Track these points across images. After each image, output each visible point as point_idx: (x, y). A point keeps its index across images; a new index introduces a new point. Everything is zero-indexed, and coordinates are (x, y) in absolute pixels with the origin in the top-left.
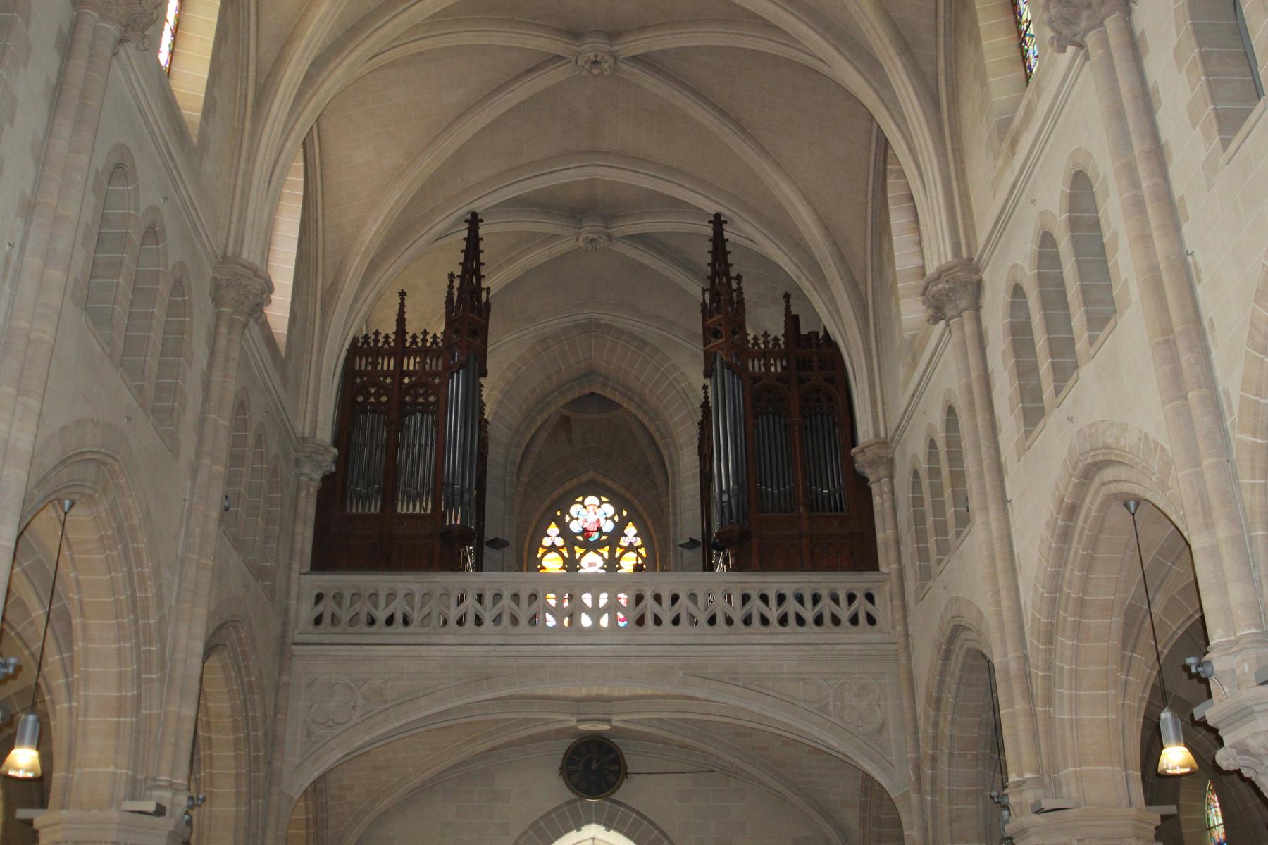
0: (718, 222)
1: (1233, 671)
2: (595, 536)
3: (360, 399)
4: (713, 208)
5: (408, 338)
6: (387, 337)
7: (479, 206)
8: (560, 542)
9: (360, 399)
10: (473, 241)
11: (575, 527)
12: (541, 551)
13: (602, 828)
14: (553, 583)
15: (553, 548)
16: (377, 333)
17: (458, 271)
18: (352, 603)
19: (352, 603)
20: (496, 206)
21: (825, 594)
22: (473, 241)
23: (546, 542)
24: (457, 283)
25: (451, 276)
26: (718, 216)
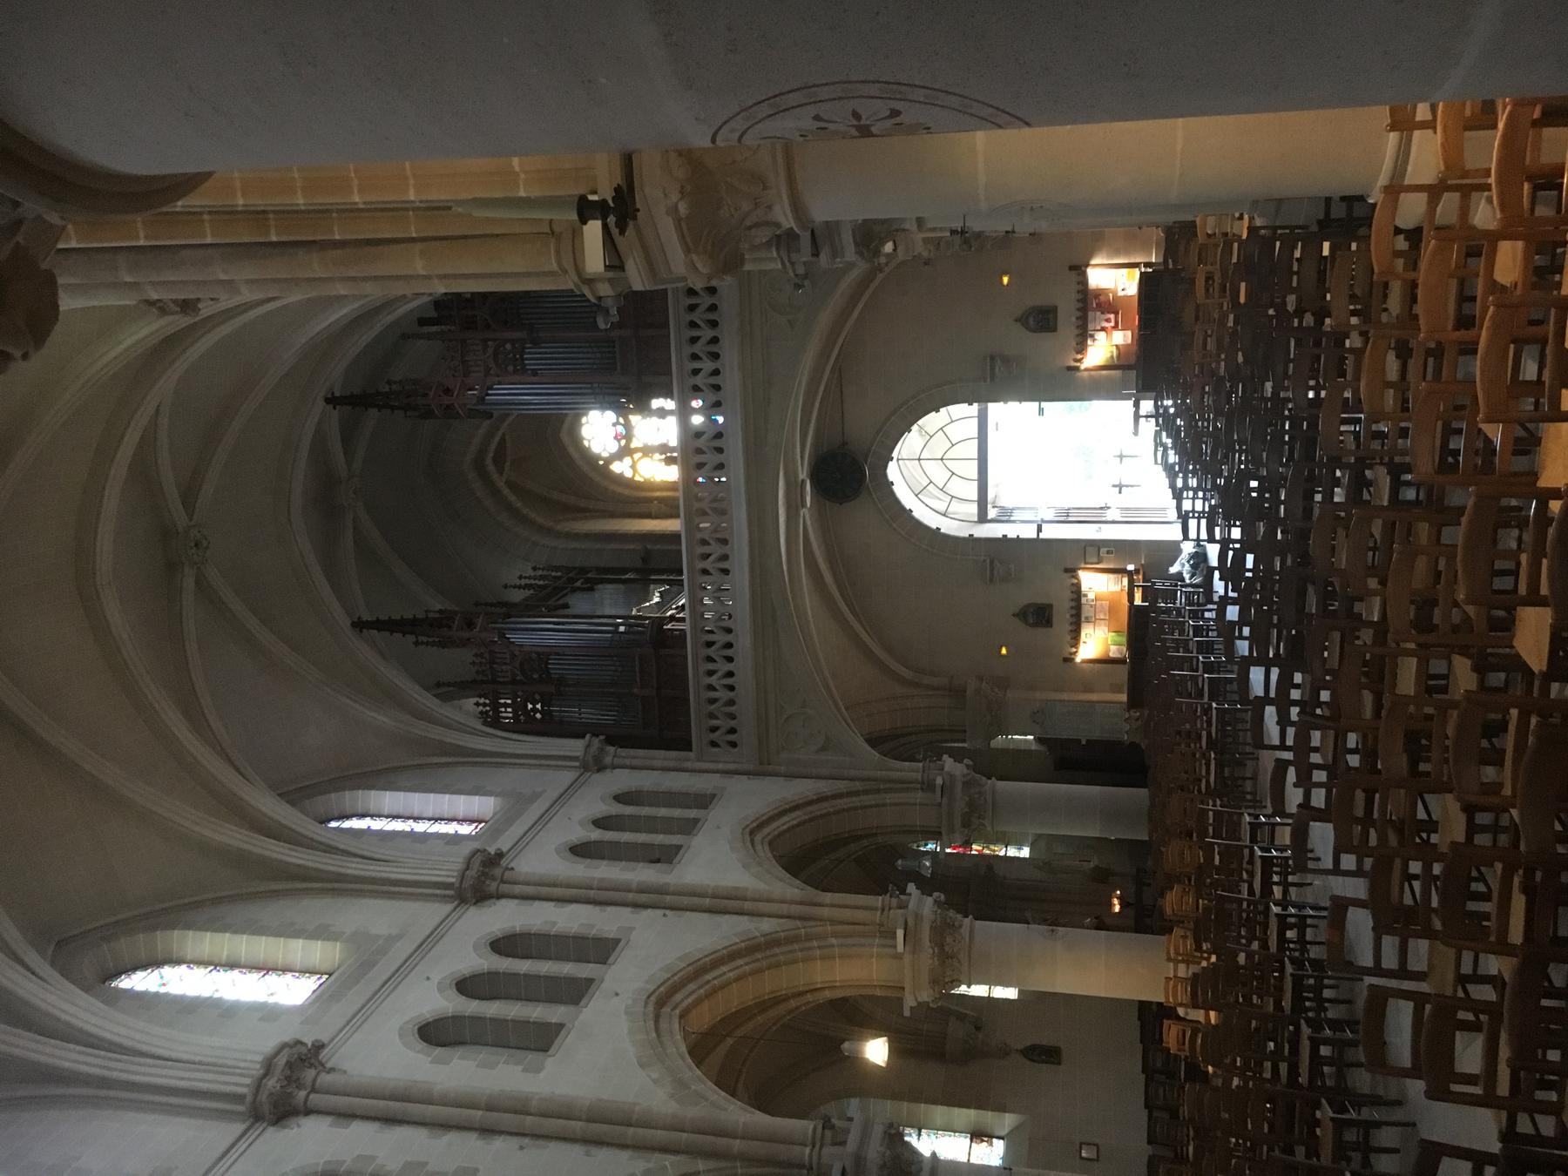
0: (331, 400)
1: (1386, 310)
2: (621, 429)
3: (538, 716)
4: (320, 403)
5: (480, 677)
6: (476, 655)
7: (345, 622)
8: (627, 461)
9: (538, 716)
10: (379, 625)
11: (613, 447)
12: (637, 478)
13: (916, 514)
14: (690, 526)
15: (633, 467)
16: (473, 663)
17: (411, 638)
18: (715, 689)
19: (715, 689)
20: (345, 453)
21: (689, 317)
22: (379, 625)
23: (628, 474)
24: (425, 639)
25: (417, 643)
26: (328, 401)
